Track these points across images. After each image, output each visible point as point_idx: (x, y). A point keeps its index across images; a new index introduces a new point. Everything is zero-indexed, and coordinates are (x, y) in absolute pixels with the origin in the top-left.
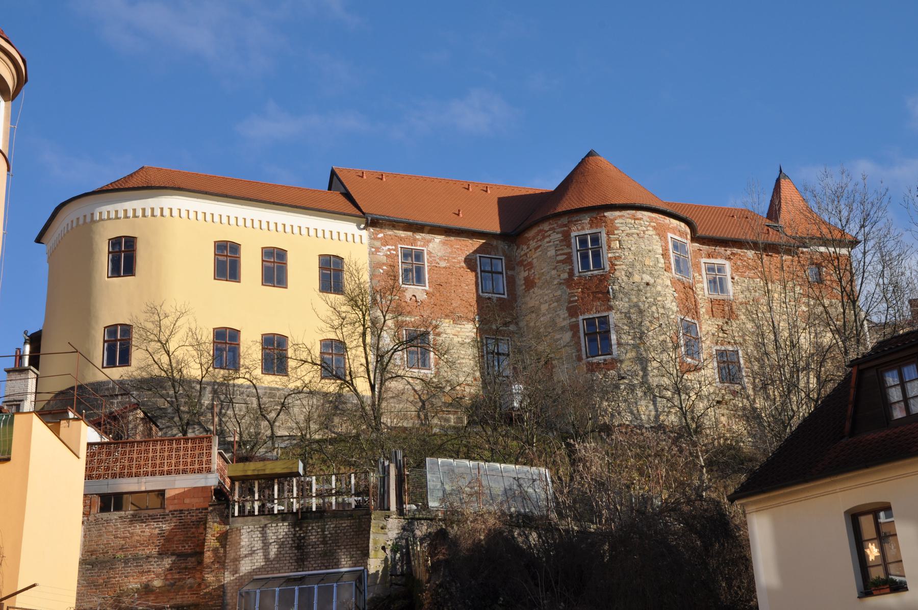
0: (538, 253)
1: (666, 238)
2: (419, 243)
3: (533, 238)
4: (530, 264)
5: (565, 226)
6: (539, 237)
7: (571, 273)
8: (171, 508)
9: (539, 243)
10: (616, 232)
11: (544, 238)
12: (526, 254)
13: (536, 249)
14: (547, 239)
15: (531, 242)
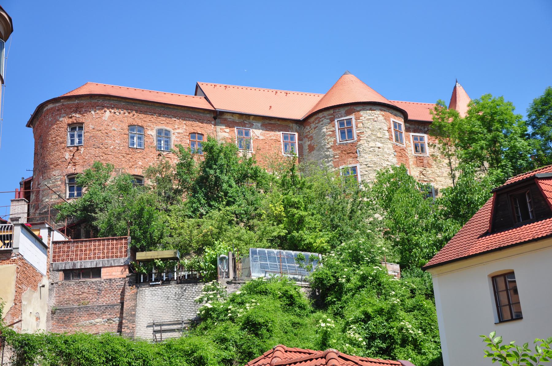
0: (316, 130)
1: (389, 121)
2: (247, 125)
3: (313, 122)
4: (311, 137)
5: (332, 114)
6: (317, 122)
7: (335, 141)
8: (105, 278)
9: (317, 125)
10: (361, 118)
11: (319, 122)
12: (309, 132)
13: (315, 128)
14: (321, 123)
15: (312, 124)
